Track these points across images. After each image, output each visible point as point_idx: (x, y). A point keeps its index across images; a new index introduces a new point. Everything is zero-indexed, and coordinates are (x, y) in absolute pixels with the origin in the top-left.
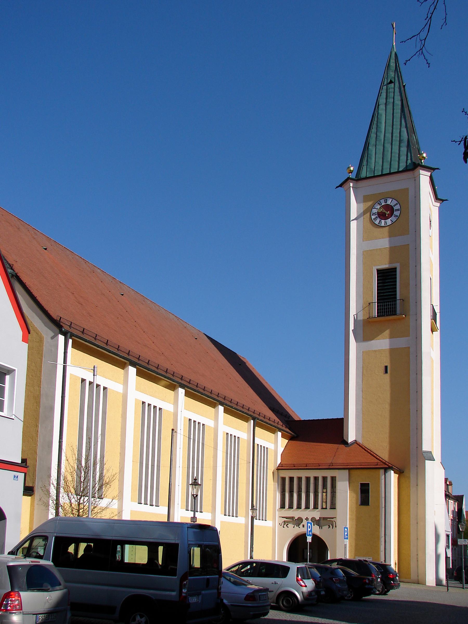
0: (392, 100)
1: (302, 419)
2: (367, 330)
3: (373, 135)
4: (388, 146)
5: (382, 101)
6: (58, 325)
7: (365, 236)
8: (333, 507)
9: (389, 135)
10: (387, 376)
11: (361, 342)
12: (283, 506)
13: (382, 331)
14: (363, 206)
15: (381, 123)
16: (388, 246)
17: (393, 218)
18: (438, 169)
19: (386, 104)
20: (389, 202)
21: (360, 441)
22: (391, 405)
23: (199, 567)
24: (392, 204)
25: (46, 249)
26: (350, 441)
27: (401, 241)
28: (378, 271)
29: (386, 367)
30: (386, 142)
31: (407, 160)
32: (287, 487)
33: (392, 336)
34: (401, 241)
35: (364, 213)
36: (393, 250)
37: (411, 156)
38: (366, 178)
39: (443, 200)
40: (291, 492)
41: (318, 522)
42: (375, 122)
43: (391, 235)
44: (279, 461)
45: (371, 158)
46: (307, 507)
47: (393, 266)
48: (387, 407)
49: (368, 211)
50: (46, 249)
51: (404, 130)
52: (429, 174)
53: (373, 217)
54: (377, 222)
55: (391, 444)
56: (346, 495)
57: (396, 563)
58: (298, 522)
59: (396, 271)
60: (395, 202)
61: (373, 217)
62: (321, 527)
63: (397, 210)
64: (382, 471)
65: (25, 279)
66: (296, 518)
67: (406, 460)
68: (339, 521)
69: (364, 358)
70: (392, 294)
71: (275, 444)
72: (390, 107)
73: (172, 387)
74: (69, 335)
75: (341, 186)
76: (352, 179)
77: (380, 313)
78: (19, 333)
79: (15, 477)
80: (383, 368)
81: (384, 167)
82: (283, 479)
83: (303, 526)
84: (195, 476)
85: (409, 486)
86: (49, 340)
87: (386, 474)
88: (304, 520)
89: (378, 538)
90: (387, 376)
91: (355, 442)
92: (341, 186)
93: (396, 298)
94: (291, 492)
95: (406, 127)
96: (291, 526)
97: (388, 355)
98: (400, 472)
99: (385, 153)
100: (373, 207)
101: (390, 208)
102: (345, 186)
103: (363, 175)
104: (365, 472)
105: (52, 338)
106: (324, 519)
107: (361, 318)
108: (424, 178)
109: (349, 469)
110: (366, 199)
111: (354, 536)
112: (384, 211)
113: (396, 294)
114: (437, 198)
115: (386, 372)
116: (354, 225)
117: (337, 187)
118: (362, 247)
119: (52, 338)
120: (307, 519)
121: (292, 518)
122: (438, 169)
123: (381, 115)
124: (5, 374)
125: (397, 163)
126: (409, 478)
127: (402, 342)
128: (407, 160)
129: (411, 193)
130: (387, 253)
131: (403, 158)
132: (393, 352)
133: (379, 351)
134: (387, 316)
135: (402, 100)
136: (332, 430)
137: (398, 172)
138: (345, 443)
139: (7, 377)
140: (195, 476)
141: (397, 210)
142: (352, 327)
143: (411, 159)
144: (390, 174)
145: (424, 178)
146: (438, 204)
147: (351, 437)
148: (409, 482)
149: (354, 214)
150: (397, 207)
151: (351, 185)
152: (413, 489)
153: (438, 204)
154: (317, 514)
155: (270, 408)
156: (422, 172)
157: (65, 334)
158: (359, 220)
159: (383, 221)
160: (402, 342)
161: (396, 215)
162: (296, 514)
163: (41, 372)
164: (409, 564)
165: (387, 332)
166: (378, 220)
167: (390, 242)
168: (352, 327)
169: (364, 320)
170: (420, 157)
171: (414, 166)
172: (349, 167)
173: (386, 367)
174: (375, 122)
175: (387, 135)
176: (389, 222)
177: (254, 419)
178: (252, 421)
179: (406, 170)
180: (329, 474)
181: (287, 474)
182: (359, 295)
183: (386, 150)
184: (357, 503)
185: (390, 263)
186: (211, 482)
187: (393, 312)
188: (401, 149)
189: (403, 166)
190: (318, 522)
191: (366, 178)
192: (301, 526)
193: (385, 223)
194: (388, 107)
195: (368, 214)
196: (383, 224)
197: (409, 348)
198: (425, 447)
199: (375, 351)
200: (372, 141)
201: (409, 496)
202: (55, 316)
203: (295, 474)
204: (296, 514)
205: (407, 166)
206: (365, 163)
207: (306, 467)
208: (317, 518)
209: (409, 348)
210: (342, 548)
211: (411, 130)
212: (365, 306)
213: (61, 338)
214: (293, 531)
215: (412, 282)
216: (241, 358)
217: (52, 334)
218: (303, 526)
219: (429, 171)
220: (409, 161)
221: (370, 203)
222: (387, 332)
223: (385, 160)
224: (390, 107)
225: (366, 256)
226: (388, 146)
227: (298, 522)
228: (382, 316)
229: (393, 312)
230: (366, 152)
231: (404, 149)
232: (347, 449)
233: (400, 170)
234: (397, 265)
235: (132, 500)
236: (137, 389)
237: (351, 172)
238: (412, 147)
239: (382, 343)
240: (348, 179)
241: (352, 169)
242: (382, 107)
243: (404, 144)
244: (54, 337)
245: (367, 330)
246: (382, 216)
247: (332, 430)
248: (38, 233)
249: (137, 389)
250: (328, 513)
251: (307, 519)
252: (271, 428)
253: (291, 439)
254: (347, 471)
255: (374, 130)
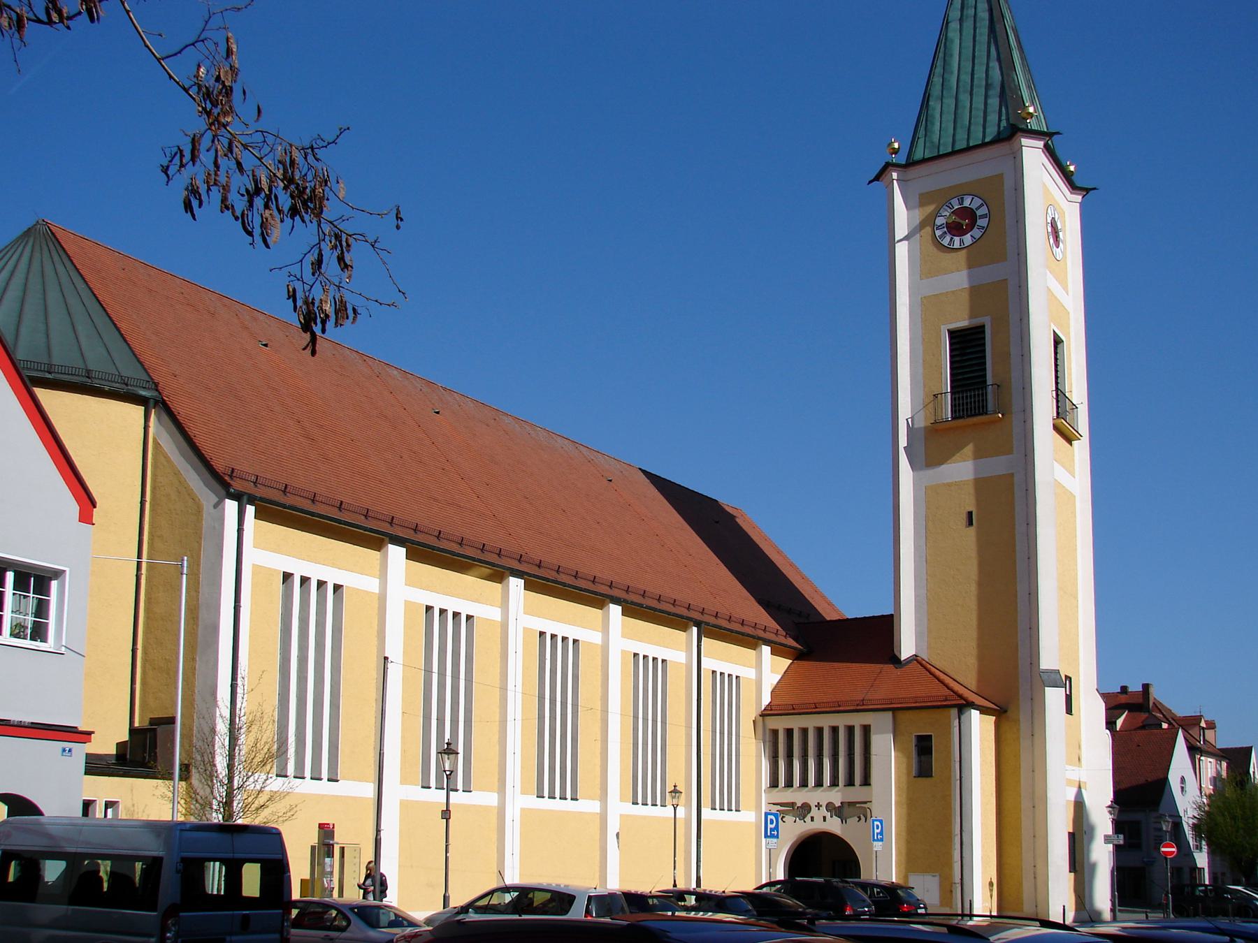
0: (972, 12)
1: (850, 615)
2: (932, 445)
3: (937, 80)
4: (964, 98)
5: (955, 14)
6: (225, 484)
7: (922, 270)
8: (866, 782)
9: (966, 78)
10: (972, 531)
11: (921, 469)
12: (774, 784)
13: (959, 448)
14: (919, 215)
15: (951, 55)
16: (966, 285)
17: (976, 232)
18: (1058, 133)
19: (961, 20)
20: (967, 203)
21: (924, 656)
22: (980, 584)
23: (257, 895)
24: (973, 206)
25: (266, 345)
26: (904, 656)
27: (990, 273)
28: (952, 334)
29: (970, 514)
30: (961, 90)
31: (1000, 120)
32: (784, 748)
33: (978, 455)
34: (990, 273)
35: (922, 225)
36: (976, 292)
37: (1007, 114)
38: (924, 161)
39: (1087, 190)
40: (790, 756)
41: (838, 811)
42: (941, 55)
43: (971, 264)
44: (766, 700)
45: (933, 124)
46: (819, 784)
47: (977, 322)
48: (973, 588)
49: (928, 222)
50: (266, 345)
51: (994, 65)
52: (1041, 144)
53: (938, 233)
54: (946, 242)
55: (981, 658)
56: (889, 760)
57: (991, 884)
58: (803, 811)
59: (984, 332)
60: (978, 202)
61: (938, 233)
62: (844, 820)
63: (982, 217)
64: (954, 712)
65: (175, 407)
66: (799, 804)
67: (1012, 688)
68: (876, 810)
69: (929, 500)
70: (980, 374)
71: (762, 672)
72: (968, 24)
73: (498, 575)
74: (245, 498)
75: (877, 178)
76: (897, 166)
77: (958, 412)
78: (74, 508)
79: (64, 750)
80: (965, 516)
81: (958, 137)
82: (775, 733)
83: (812, 819)
84: (447, 736)
85: (1018, 738)
86: (212, 510)
87: (963, 717)
88: (813, 808)
89: (950, 837)
90: (972, 531)
91: (915, 658)
92: (877, 178)
93: (985, 382)
94: (790, 756)
95: (999, 60)
96: (789, 819)
97: (972, 491)
98: (1000, 711)
99: (959, 111)
100: (937, 214)
101: (970, 215)
102: (885, 178)
103: (918, 155)
104: (924, 714)
105: (216, 506)
106: (851, 804)
107: (921, 423)
108: (1033, 155)
109: (894, 710)
110: (924, 199)
111: (904, 834)
112: (958, 220)
113: (985, 376)
114: (1073, 187)
115: (970, 523)
116: (902, 251)
117: (870, 182)
118: (916, 289)
119: (216, 506)
120: (818, 806)
121: (793, 804)
122: (1058, 133)
123: (952, 41)
124: (51, 579)
125: (981, 129)
126: (1017, 721)
127: (998, 465)
128: (1000, 120)
129: (1008, 183)
130: (965, 297)
131: (993, 118)
132: (982, 485)
133: (956, 484)
134: (968, 416)
135: (991, 11)
136: (875, 636)
137: (984, 145)
138: (895, 660)
139: (54, 584)
140: (447, 736)
141: (982, 217)
142: (903, 442)
143: (1008, 119)
144: (969, 149)
145: (1033, 155)
146: (1079, 198)
147: (907, 648)
148: (1018, 730)
149: (901, 228)
150: (984, 210)
151: (895, 175)
152: (1024, 743)
153: (1079, 198)
154: (836, 796)
155: (760, 602)
156: (1024, 141)
157: (237, 497)
158: (912, 239)
159: (957, 239)
160: (998, 465)
161: (983, 228)
162: (798, 796)
163: (199, 565)
164: (1021, 884)
165: (969, 450)
166: (948, 238)
167: (970, 277)
168: (903, 442)
169: (926, 428)
170: (1024, 115)
171: (1013, 131)
172: (891, 144)
173: (970, 514)
174: (941, 55)
175: (962, 77)
176: (968, 239)
177: (698, 624)
178: (695, 629)
179: (998, 140)
180: (857, 720)
181: (780, 724)
182: (914, 379)
183: (960, 104)
184: (908, 774)
185: (972, 316)
186: (599, 744)
187: (981, 409)
188: (989, 101)
189: (991, 133)
190: (838, 811)
191: (924, 161)
192: (808, 819)
193: (962, 242)
194: (965, 25)
195: (928, 229)
196: (957, 245)
197: (1012, 475)
198: (1048, 660)
199: (949, 485)
200: (936, 90)
201: (1017, 756)
202: (220, 465)
203: (796, 723)
204: (798, 796)
205: (999, 133)
206: (921, 132)
207: (815, 710)
208: (838, 804)
209: (1012, 475)
210: (884, 861)
211: (1007, 66)
212: (927, 401)
213: (231, 506)
214: (792, 830)
215: (1014, 351)
216: (727, 509)
217: (215, 499)
218: (812, 819)
219: (1040, 140)
220: (1004, 123)
221: (930, 209)
222: (969, 450)
223: (958, 125)
224: (968, 24)
225: (926, 307)
226: (964, 98)
227: (803, 811)
228: (960, 417)
229: (981, 409)
230: (924, 111)
231: (994, 102)
232: (899, 672)
233: (987, 140)
234: (986, 321)
235: (404, 780)
236: (409, 582)
237: (895, 152)
238: (1008, 95)
239: (961, 470)
240: (887, 166)
241: (896, 145)
242: (954, 26)
243: (995, 91)
244: (219, 505)
245: (932, 445)
246: (955, 229)
247: (875, 636)
248: (262, 317)
249: (409, 582)
250: (856, 793)
251: (818, 806)
252: (747, 638)
253: (798, 656)
254: (889, 715)
255: (939, 70)
